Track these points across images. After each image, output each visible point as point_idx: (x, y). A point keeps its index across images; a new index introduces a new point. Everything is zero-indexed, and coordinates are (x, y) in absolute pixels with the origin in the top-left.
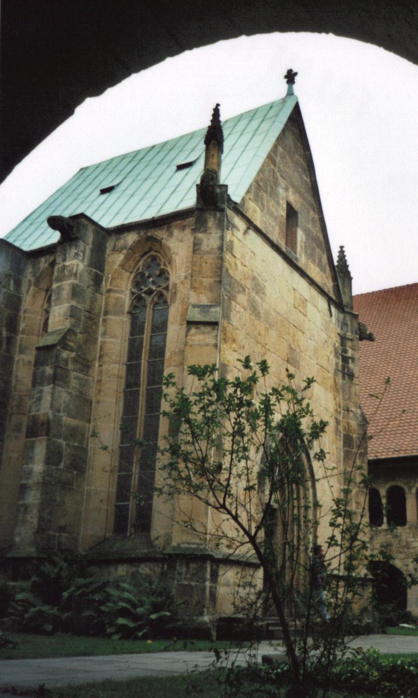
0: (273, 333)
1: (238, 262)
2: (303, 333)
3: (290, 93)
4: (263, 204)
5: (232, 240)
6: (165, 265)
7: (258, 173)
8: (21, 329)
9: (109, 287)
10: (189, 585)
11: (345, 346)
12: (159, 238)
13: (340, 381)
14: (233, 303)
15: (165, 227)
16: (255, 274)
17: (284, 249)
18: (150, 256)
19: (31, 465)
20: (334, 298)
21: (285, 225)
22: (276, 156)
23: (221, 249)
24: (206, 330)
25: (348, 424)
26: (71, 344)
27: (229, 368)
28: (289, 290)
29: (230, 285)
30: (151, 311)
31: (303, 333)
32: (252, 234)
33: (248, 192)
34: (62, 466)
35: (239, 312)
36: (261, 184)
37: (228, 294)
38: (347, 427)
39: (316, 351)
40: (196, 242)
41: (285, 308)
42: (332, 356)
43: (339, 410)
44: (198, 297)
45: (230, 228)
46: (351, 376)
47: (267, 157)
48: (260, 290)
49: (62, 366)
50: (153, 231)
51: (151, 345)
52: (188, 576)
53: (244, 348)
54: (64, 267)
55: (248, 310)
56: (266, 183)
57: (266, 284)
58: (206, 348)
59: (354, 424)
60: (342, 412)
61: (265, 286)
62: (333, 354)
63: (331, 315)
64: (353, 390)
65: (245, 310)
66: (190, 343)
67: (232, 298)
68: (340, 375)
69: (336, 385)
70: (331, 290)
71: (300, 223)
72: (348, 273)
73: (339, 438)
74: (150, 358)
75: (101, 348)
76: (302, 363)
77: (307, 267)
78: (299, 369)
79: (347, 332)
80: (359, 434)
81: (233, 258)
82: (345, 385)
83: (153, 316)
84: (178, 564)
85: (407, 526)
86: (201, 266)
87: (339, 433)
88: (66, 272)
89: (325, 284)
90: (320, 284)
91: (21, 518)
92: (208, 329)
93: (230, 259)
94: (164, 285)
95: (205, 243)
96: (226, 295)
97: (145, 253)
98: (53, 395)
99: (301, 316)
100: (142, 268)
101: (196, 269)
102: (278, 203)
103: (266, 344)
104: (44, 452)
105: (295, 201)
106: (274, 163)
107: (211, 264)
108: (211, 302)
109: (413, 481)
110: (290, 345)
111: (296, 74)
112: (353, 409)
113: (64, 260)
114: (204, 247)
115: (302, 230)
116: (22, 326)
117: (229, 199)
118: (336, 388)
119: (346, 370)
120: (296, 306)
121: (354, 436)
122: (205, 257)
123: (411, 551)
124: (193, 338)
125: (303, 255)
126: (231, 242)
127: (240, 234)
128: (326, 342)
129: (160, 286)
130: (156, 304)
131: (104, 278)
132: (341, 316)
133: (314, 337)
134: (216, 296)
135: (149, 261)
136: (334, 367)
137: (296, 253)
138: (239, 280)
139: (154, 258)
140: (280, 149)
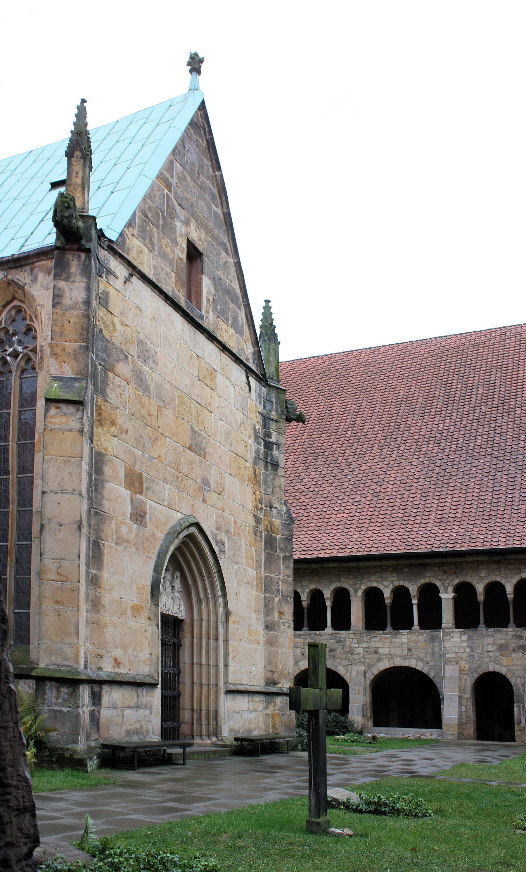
0: (168, 413)
1: (116, 321)
2: (211, 412)
3: (194, 89)
4: (153, 244)
5: (107, 290)
6: (31, 320)
7: (144, 200)
10: (61, 711)
11: (269, 429)
12: (21, 283)
13: (261, 470)
14: (111, 375)
15: (28, 268)
16: (142, 336)
17: (183, 303)
18: (14, 307)
20: (254, 368)
21: (185, 271)
22: (172, 177)
23: (88, 303)
24: (69, 411)
25: (271, 522)
27: (107, 458)
28: (191, 357)
29: (105, 351)
30: (18, 380)
31: (211, 412)
32: (136, 281)
33: (130, 224)
35: (119, 386)
36: (150, 215)
37: (103, 364)
38: (269, 526)
39: (228, 434)
40: (56, 292)
41: (186, 380)
42: (251, 441)
43: (260, 506)
44: (61, 367)
45: (104, 275)
46: (275, 465)
47: (158, 177)
48: (149, 358)
50: (14, 271)
51: (20, 422)
52: (59, 701)
53: (127, 432)
55: (132, 384)
56: (158, 214)
57: (158, 350)
58: (70, 433)
59: (277, 522)
60: (264, 508)
61: (156, 352)
62: (253, 438)
63: (250, 390)
64: (277, 482)
65: (128, 383)
66: (50, 426)
67: (108, 368)
68: (262, 464)
69: (256, 476)
70: (251, 357)
71: (205, 271)
72: (275, 335)
73: (259, 538)
74: (19, 440)
76: (209, 450)
77: (217, 326)
78: (205, 458)
79: (271, 411)
81: (109, 315)
82: (267, 476)
83: (21, 385)
84: (47, 687)
85: (351, 632)
86: (63, 325)
87: (258, 534)
89: (243, 350)
90: (234, 351)
92: (71, 409)
93: (104, 317)
94: (31, 347)
95: (67, 294)
96: (100, 365)
97: (8, 303)
99: (208, 390)
100: (5, 322)
101: (57, 329)
102: (174, 241)
103: (159, 427)
105: (200, 240)
106: (169, 186)
107: (75, 323)
108: (77, 374)
109: (359, 582)
110: (192, 428)
111: (201, 61)
114: (67, 301)
115: (210, 279)
117: (101, 234)
118: (256, 480)
119: (269, 459)
120: (201, 379)
121: (278, 537)
122: (68, 314)
123: (355, 657)
124: (53, 420)
125: (211, 313)
126: (106, 294)
127: (119, 284)
128: (242, 423)
129: (26, 347)
130: (23, 371)
132: (265, 390)
133: (226, 418)
134: (82, 365)
135: (13, 312)
136: (253, 454)
137: (200, 309)
138: (118, 345)
139: (19, 310)
140: (177, 166)
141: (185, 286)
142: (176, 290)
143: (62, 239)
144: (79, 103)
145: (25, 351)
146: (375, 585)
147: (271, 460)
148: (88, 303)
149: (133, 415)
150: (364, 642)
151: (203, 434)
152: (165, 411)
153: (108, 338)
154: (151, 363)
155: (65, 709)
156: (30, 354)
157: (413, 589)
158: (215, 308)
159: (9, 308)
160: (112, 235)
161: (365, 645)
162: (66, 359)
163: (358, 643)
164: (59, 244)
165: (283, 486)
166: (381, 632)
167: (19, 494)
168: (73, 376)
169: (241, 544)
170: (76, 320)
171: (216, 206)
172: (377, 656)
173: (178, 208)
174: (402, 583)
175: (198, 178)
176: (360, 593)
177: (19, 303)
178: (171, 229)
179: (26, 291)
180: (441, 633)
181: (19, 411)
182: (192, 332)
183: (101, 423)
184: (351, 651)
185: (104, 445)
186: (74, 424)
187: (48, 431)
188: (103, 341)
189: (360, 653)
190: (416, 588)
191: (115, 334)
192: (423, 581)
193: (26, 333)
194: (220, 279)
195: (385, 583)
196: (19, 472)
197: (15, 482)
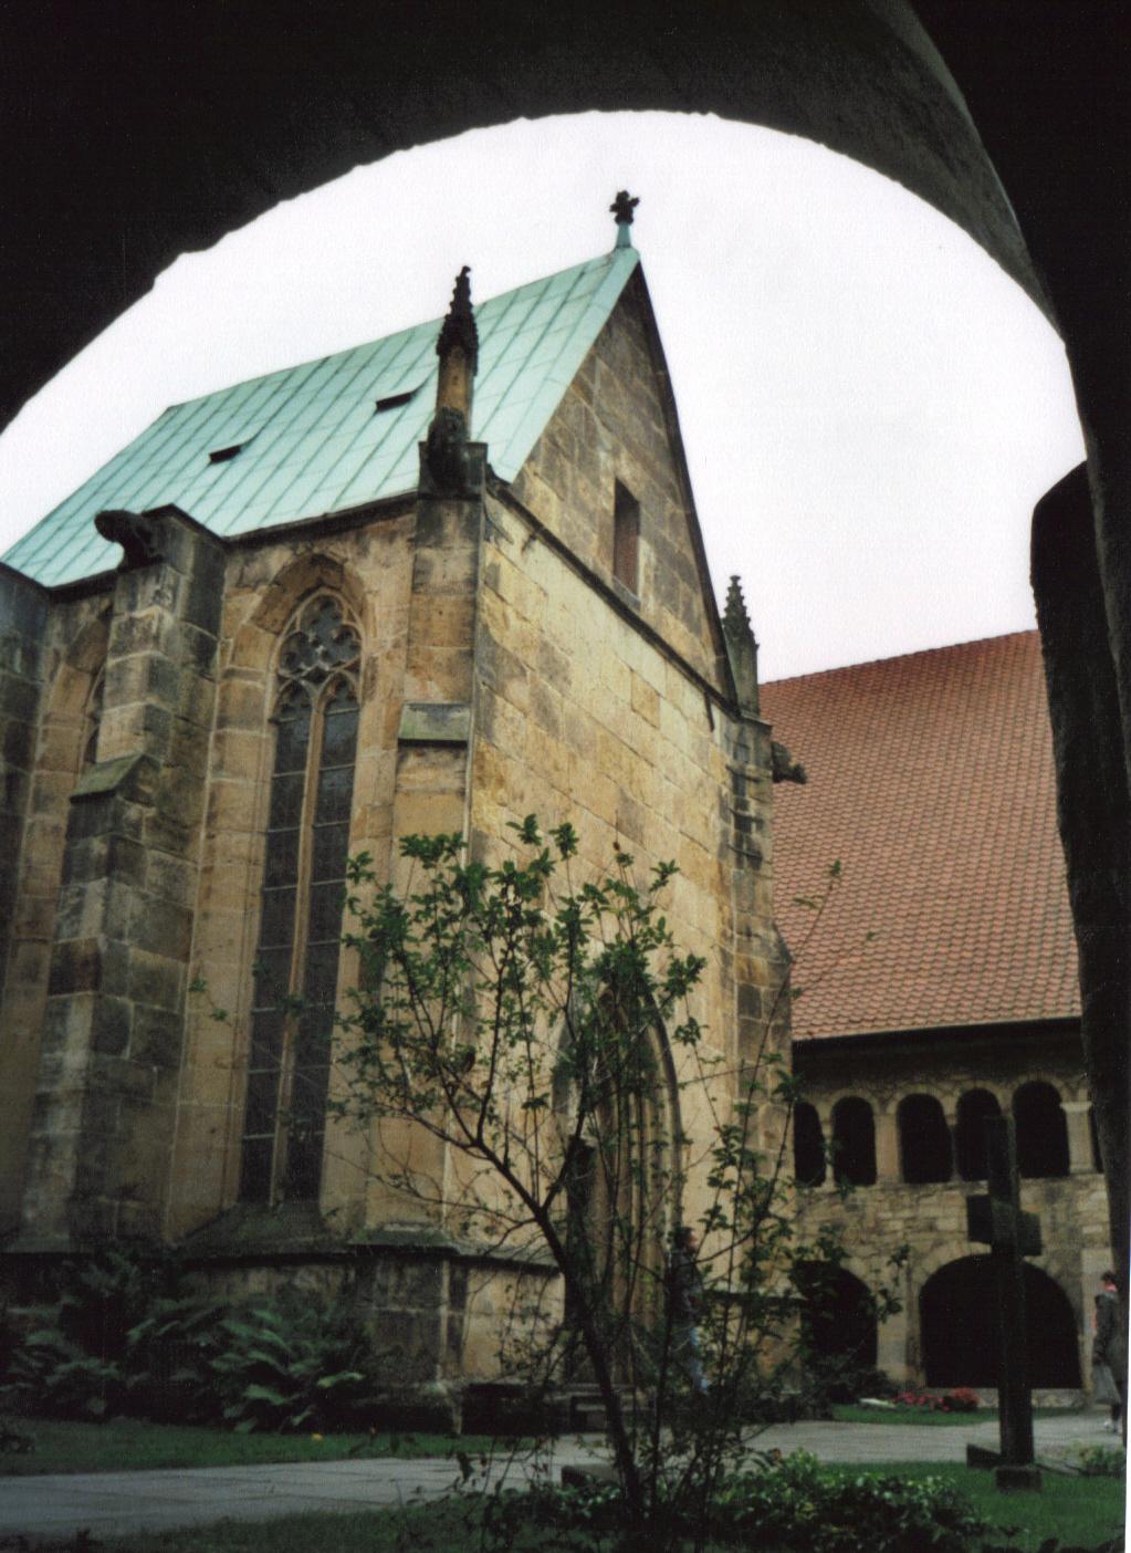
0: (586, 766)
1: (510, 611)
2: (652, 765)
3: (623, 244)
4: (563, 486)
6: (351, 618)
7: (553, 419)
8: (37, 757)
9: (228, 666)
10: (403, 1315)
11: (744, 794)
12: (338, 560)
14: (499, 700)
16: (547, 638)
18: (318, 598)
19: (58, 1054)
20: (718, 688)
22: (593, 382)
23: (473, 582)
25: (749, 964)
26: (147, 789)
28: (621, 671)
29: (492, 661)
30: (322, 718)
31: (652, 765)
32: (540, 550)
33: (532, 458)
34: (127, 1054)
35: (512, 720)
36: (560, 441)
37: (488, 682)
38: (746, 969)
39: (679, 803)
40: (419, 567)
42: (714, 816)
43: (729, 932)
44: (424, 686)
45: (492, 538)
48: (557, 673)
49: (127, 836)
53: (522, 797)
54: (132, 622)
55: (532, 715)
56: (572, 440)
57: (570, 659)
58: (440, 797)
59: (761, 962)
60: (736, 936)
62: (717, 810)
63: (712, 727)
66: (406, 787)
67: (497, 689)
68: (732, 856)
69: (722, 879)
70: (712, 672)
71: (644, 527)
72: (750, 634)
73: (728, 993)
74: (317, 819)
75: (213, 798)
76: (649, 831)
78: (641, 843)
79: (747, 762)
80: (772, 985)
81: (499, 601)
82: (741, 878)
83: (325, 729)
86: (429, 619)
87: (728, 984)
88: (137, 634)
89: (700, 658)
90: (687, 659)
91: (38, 1167)
92: (446, 756)
93: (492, 605)
94: (349, 662)
95: (438, 570)
97: (309, 592)
98: (107, 899)
100: (302, 624)
101: (418, 626)
102: (596, 483)
103: (571, 790)
104: (89, 1025)
105: (634, 479)
106: (588, 396)
107: (451, 615)
110: (622, 791)
111: (635, 202)
112: (760, 931)
113: (132, 607)
114: (436, 579)
115: (649, 542)
116: (40, 749)
117: (491, 475)
118: (722, 886)
119: (745, 846)
121: (763, 989)
123: (887, 1239)
124: (412, 776)
125: (651, 597)
126: (495, 568)
127: (513, 551)
128: (700, 784)
129: (339, 664)
130: (330, 703)
131: (219, 646)
132: (734, 728)
134: (461, 683)
135: (316, 608)
136: (718, 839)
137: (635, 592)
138: (511, 650)
139: (327, 603)
140: (601, 365)
141: (611, 555)
142: (599, 562)
143: (431, 481)
144: (458, 272)
145: (338, 670)
146: (922, 1090)
147: (749, 849)
148: (473, 582)
149: (532, 769)
150: (904, 1207)
151: (640, 803)
152: (580, 762)
153: (497, 639)
154: (560, 681)
155: (413, 1311)
156: (349, 675)
157: (1004, 1096)
158: (657, 590)
159: (309, 600)
160: (506, 470)
161: (907, 1213)
162: (433, 674)
163: (892, 1209)
164: (426, 490)
165: (770, 896)
166: (940, 1186)
167: (312, 916)
168: (446, 702)
169: (700, 1003)
170: (454, 610)
171: (659, 425)
172: (933, 1236)
173: (602, 432)
174: (980, 1084)
175: (631, 382)
176: (892, 1108)
177: (327, 592)
178: (591, 463)
179: (345, 573)
180: (1066, 1186)
181: (321, 773)
182: (623, 631)
183: (482, 781)
184: (878, 1229)
185: (486, 819)
186: (450, 780)
187: (400, 796)
188: (489, 645)
189: (895, 1232)
190: (1010, 1096)
191: (507, 633)
192: (1023, 1080)
193: (340, 640)
194: (664, 540)
195: (947, 1087)
196: (315, 877)
197: (307, 892)
